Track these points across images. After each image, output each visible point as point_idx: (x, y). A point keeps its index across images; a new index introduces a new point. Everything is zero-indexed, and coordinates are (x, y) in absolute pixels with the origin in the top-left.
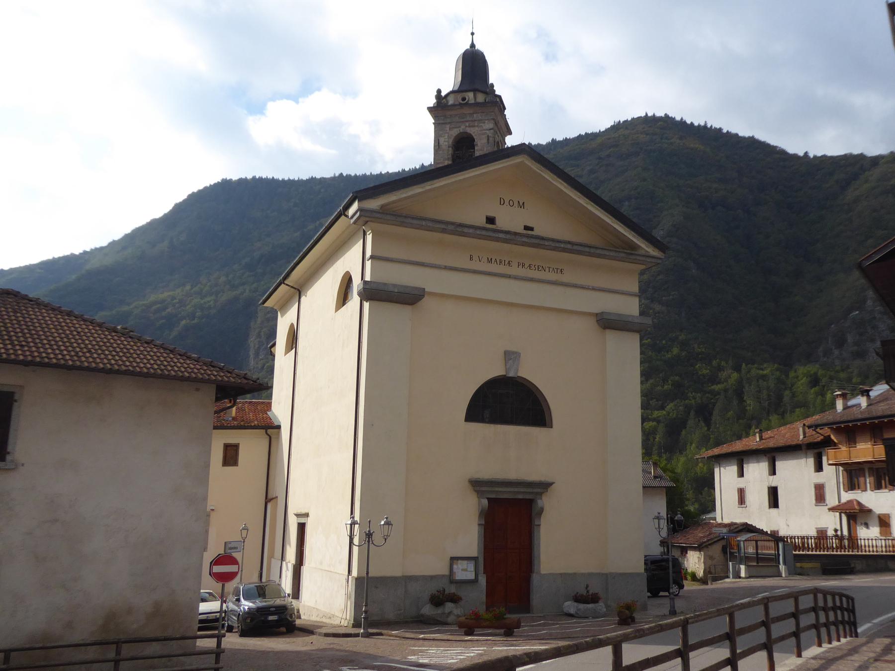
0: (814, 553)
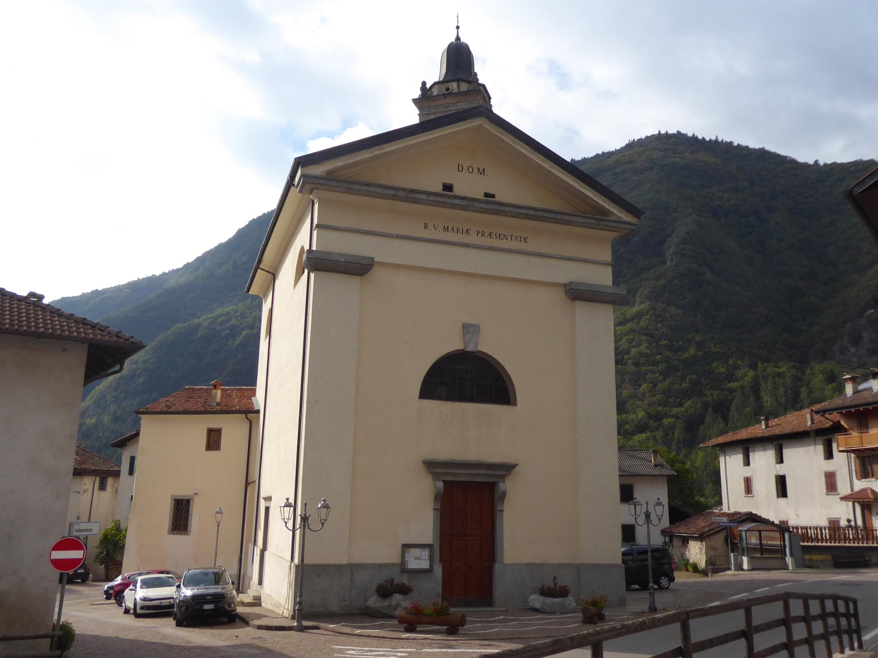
0: (829, 544)
